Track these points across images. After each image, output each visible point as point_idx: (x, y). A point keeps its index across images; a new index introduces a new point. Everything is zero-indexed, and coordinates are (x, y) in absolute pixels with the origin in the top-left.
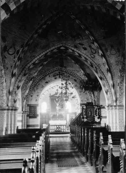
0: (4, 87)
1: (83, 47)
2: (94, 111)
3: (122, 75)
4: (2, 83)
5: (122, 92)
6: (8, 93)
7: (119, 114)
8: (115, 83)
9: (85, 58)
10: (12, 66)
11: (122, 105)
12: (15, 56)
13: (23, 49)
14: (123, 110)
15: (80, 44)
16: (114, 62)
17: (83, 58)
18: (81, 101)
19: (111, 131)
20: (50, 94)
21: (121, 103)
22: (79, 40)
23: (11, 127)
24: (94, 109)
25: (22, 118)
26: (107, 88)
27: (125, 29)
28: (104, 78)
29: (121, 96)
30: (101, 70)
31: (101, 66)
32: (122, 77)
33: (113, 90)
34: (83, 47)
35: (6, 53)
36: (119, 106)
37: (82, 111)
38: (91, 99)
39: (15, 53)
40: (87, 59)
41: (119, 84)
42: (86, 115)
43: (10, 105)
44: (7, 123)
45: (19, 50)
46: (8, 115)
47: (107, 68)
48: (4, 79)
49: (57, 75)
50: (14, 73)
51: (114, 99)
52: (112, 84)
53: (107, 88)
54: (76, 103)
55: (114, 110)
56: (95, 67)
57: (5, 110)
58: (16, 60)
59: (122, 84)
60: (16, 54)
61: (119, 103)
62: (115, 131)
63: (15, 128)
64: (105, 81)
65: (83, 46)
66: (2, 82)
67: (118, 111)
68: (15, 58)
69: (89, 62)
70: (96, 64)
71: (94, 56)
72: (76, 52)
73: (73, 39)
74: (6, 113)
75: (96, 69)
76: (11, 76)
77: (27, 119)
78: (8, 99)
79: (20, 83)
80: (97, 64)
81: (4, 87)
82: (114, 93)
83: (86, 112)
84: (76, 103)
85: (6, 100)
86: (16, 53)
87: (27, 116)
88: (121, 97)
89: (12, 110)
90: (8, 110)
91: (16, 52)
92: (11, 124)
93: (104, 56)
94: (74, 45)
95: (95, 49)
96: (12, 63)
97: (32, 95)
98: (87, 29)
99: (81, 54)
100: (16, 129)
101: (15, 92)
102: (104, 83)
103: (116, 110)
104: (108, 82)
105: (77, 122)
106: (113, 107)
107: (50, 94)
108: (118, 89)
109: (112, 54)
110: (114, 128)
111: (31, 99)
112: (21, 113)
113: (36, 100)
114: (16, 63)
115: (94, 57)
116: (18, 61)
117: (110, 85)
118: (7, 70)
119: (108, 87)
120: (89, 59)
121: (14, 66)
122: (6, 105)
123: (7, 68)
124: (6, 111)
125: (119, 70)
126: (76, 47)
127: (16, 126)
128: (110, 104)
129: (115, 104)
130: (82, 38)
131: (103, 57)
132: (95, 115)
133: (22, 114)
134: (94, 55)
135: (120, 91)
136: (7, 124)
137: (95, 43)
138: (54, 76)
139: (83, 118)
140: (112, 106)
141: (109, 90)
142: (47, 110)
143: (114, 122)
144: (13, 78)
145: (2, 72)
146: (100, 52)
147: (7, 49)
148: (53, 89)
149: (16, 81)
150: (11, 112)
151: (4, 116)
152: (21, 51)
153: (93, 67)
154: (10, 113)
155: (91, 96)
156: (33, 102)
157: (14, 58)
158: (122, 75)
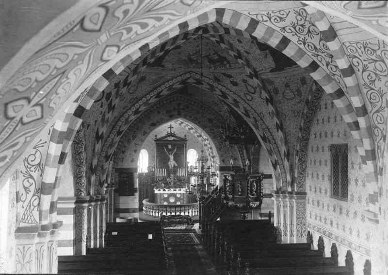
0: (82, 161)
1: (231, 81)
4: (80, 153)
5: (304, 167)
6: (89, 171)
7: (298, 207)
9: (235, 100)
10: (96, 121)
11: (303, 191)
12: (102, 103)
14: (304, 201)
15: (224, 74)
21: (301, 189)
27: (346, 255)
28: (270, 138)
29: (301, 174)
30: (264, 123)
31: (265, 117)
33: (286, 163)
34: (231, 81)
37: (225, 184)
38: (241, 157)
39: (102, 98)
40: (238, 102)
41: (299, 153)
44: (88, 226)
45: (110, 93)
47: (277, 123)
48: (83, 147)
50: (100, 133)
51: (289, 178)
52: (285, 152)
54: (209, 154)
55: (287, 199)
56: (253, 117)
61: (297, 187)
63: (102, 230)
66: (79, 152)
67: (295, 203)
70: (255, 112)
72: (217, 89)
73: (212, 66)
75: (256, 121)
78: (89, 182)
79: (111, 148)
81: (82, 161)
82: (288, 168)
83: (232, 185)
84: (209, 154)
85: (85, 184)
86: (106, 98)
87: (116, 191)
88: (302, 176)
89: (96, 201)
90: (90, 201)
93: (270, 101)
94: (214, 76)
97: (124, 149)
99: (226, 92)
101: (102, 167)
102: (270, 147)
104: (277, 146)
105: (211, 204)
106: (287, 195)
107: (156, 136)
108: (297, 162)
109: (286, 97)
111: (123, 159)
117: (282, 153)
120: (242, 102)
123: (89, 126)
124: (86, 205)
126: (217, 79)
129: (290, 189)
130: (230, 66)
131: (269, 104)
134: (253, 95)
139: (226, 198)
140: (283, 193)
141: (280, 162)
142: (149, 167)
146: (265, 95)
153: (249, 117)
155: (241, 153)
156: (126, 165)
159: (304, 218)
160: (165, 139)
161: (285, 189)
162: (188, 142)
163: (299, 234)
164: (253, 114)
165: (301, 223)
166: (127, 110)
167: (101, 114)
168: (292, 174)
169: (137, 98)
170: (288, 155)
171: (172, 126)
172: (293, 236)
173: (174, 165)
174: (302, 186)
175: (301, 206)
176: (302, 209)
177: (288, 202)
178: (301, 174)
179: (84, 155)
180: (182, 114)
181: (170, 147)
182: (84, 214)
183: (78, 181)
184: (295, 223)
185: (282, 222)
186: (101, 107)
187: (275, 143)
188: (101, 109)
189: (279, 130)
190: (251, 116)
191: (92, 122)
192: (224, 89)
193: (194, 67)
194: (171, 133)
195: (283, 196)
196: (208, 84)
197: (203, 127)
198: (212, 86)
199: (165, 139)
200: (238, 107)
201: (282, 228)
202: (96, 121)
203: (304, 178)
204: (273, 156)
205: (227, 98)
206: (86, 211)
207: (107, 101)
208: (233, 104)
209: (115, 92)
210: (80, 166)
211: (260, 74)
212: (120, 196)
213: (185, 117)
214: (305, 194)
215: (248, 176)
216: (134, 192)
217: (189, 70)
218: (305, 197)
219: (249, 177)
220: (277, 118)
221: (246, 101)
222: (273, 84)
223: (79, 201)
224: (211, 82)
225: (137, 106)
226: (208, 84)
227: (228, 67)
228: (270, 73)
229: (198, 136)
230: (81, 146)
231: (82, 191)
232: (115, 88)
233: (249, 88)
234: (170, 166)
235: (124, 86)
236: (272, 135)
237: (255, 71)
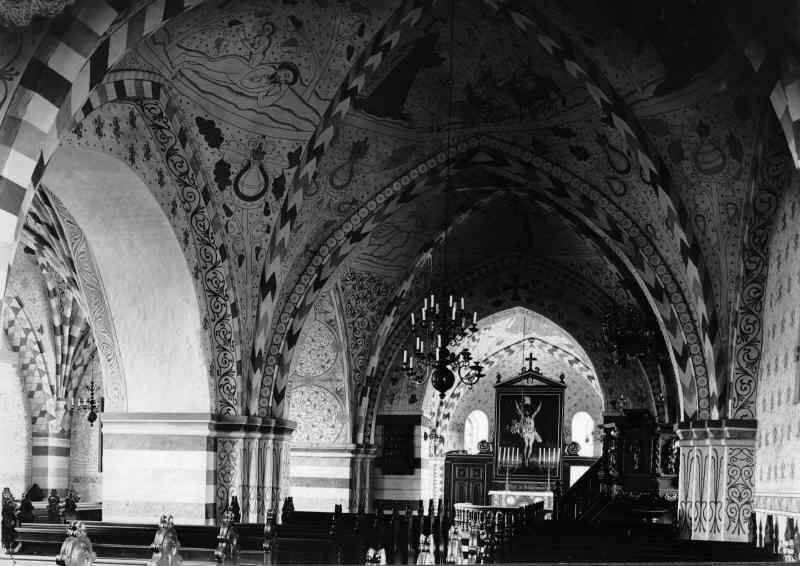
0: (228, 336)
2: (656, 450)
3: (756, 274)
5: (753, 355)
8: (722, 313)
9: (553, 180)
10: (258, 250)
11: (749, 418)
12: (267, 204)
13: (297, 174)
14: (749, 442)
16: (715, 210)
17: (575, 197)
18: (607, 408)
19: (693, 538)
20: (499, 377)
22: (551, 113)
23: (260, 498)
24: (656, 443)
25: (353, 471)
26: (682, 337)
28: (672, 288)
29: (746, 373)
31: (658, 235)
32: (754, 282)
35: (229, 190)
36: (730, 423)
40: (592, 203)
41: (740, 317)
42: (618, 467)
43: (254, 409)
44: (331, 486)
46: (246, 452)
49: (504, 290)
50: (267, 278)
51: (714, 387)
53: (682, 337)
55: (708, 442)
56: (631, 239)
57: (236, 428)
58: (274, 221)
59: (752, 319)
60: (270, 193)
62: (722, 539)
64: (675, 305)
65: (572, 141)
68: (272, 215)
69: (602, 218)
71: (625, 185)
72: (540, 175)
74: (241, 441)
75: (637, 248)
76: (257, 292)
77: (373, 478)
80: (640, 224)
81: (228, 336)
85: (239, 389)
87: (375, 463)
89: (265, 430)
90: (249, 428)
91: (271, 187)
92: (261, 487)
93: (663, 179)
95: (624, 151)
96: (260, 233)
98: (568, 51)
100: (281, 505)
103: (717, 442)
104: (688, 309)
107: (499, 377)
109: (704, 167)
110: (707, 525)
112: (349, 451)
113: (413, 400)
114: (274, 237)
115: (622, 191)
116: (282, 226)
118: (240, 265)
119: (686, 334)
121: (266, 246)
122: (239, 410)
123: (241, 258)
125: (740, 247)
126: (540, 149)
127: (282, 497)
128: (695, 414)
129: (715, 415)
132: (659, 470)
133: (350, 455)
135: (742, 352)
136: (245, 487)
137: (616, 119)
138: (491, 293)
140: (700, 424)
143: (708, 496)
144: (264, 297)
145: (219, 275)
146: (647, 164)
147: (232, 177)
148: (512, 352)
149: (280, 313)
150: (260, 439)
151: (234, 454)
152: (289, 180)
154: (255, 445)
157: (267, 212)
158: (756, 274)
159: (748, 487)
160: (519, 383)
161: (703, 415)
162: (566, 391)
163: (734, 525)
164: (628, 230)
165: (740, 498)
166: (334, 231)
167: (268, 231)
168: (722, 375)
169: (355, 202)
170: (713, 327)
171: (529, 357)
172: (719, 531)
173: (535, 441)
174: (747, 404)
175: (742, 456)
176: (745, 463)
177: (710, 448)
178: (746, 373)
179: (232, 324)
180: (523, 299)
181: (528, 401)
182: (234, 454)
183: (223, 382)
184: (723, 497)
185: (693, 498)
186: (267, 212)
187: (684, 301)
188: (266, 219)
189: (690, 262)
190: (626, 236)
191: (250, 251)
192: (557, 172)
193: (486, 120)
194: (531, 369)
195: (697, 433)
196: (521, 161)
197: (591, 352)
198: (528, 165)
199: (519, 383)
200: (592, 215)
201: (693, 514)
202: (258, 250)
203: (753, 384)
204: (678, 334)
205: (568, 196)
206: (238, 448)
207: (277, 199)
208: (580, 210)
209: (292, 177)
210: (225, 350)
211: (632, 104)
212: (384, 474)
213: (529, 304)
214: (754, 424)
215: (655, 425)
216: (414, 467)
217: (475, 130)
218: (754, 434)
219: (659, 429)
220: (683, 227)
221: (613, 197)
222: (668, 132)
223: (222, 423)
224: (527, 157)
225: (356, 221)
226: (521, 161)
227: (560, 107)
228: (655, 100)
229: (571, 362)
230: (223, 302)
231: (230, 405)
232: (291, 166)
233: (615, 157)
234: (526, 441)
235: (309, 159)
236: (674, 280)
237: (613, 93)
